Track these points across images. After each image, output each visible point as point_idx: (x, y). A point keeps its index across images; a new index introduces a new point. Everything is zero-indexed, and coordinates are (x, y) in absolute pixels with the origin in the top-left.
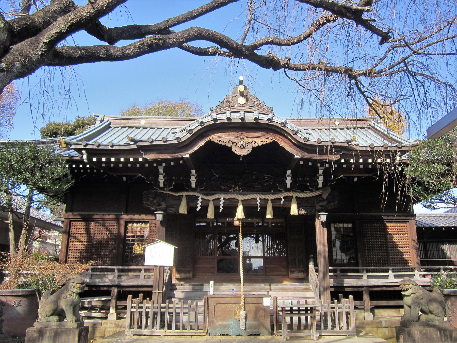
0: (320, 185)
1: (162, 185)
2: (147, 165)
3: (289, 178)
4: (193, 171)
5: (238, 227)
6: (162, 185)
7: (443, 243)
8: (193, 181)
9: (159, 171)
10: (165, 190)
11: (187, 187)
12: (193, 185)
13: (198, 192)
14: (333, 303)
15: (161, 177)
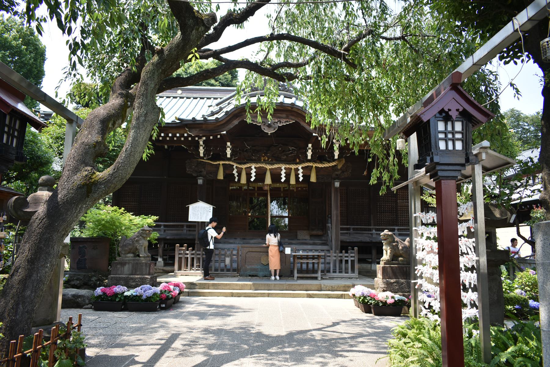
0: (336, 157)
1: (202, 155)
2: (190, 139)
3: (310, 151)
4: (229, 144)
5: (267, 191)
6: (202, 155)
7: (63, 241)
8: (229, 152)
9: (199, 143)
10: (204, 159)
11: (225, 158)
12: (229, 156)
13: (233, 161)
14: (341, 252)
15: (201, 148)
